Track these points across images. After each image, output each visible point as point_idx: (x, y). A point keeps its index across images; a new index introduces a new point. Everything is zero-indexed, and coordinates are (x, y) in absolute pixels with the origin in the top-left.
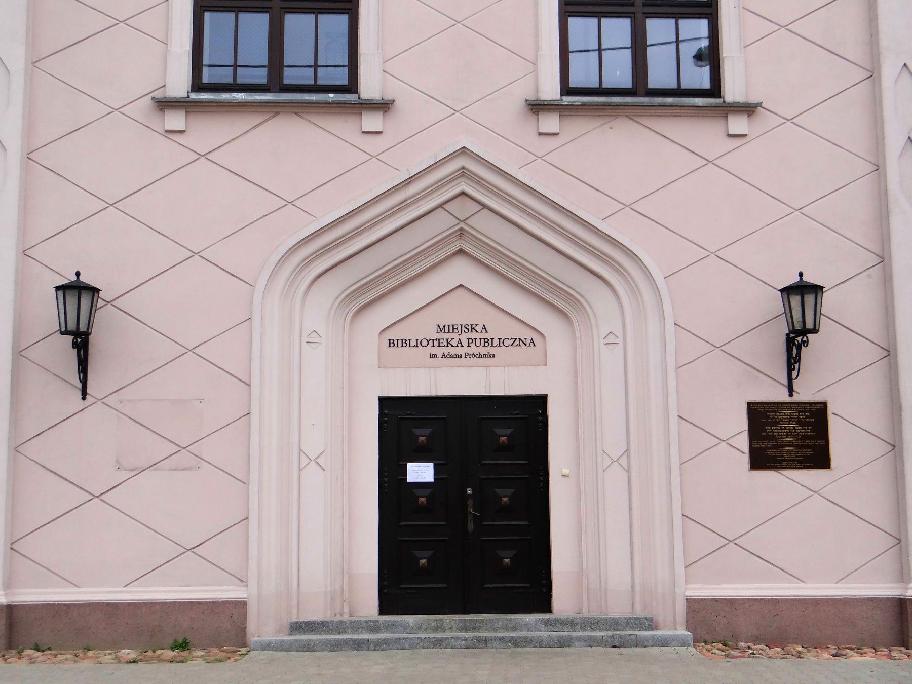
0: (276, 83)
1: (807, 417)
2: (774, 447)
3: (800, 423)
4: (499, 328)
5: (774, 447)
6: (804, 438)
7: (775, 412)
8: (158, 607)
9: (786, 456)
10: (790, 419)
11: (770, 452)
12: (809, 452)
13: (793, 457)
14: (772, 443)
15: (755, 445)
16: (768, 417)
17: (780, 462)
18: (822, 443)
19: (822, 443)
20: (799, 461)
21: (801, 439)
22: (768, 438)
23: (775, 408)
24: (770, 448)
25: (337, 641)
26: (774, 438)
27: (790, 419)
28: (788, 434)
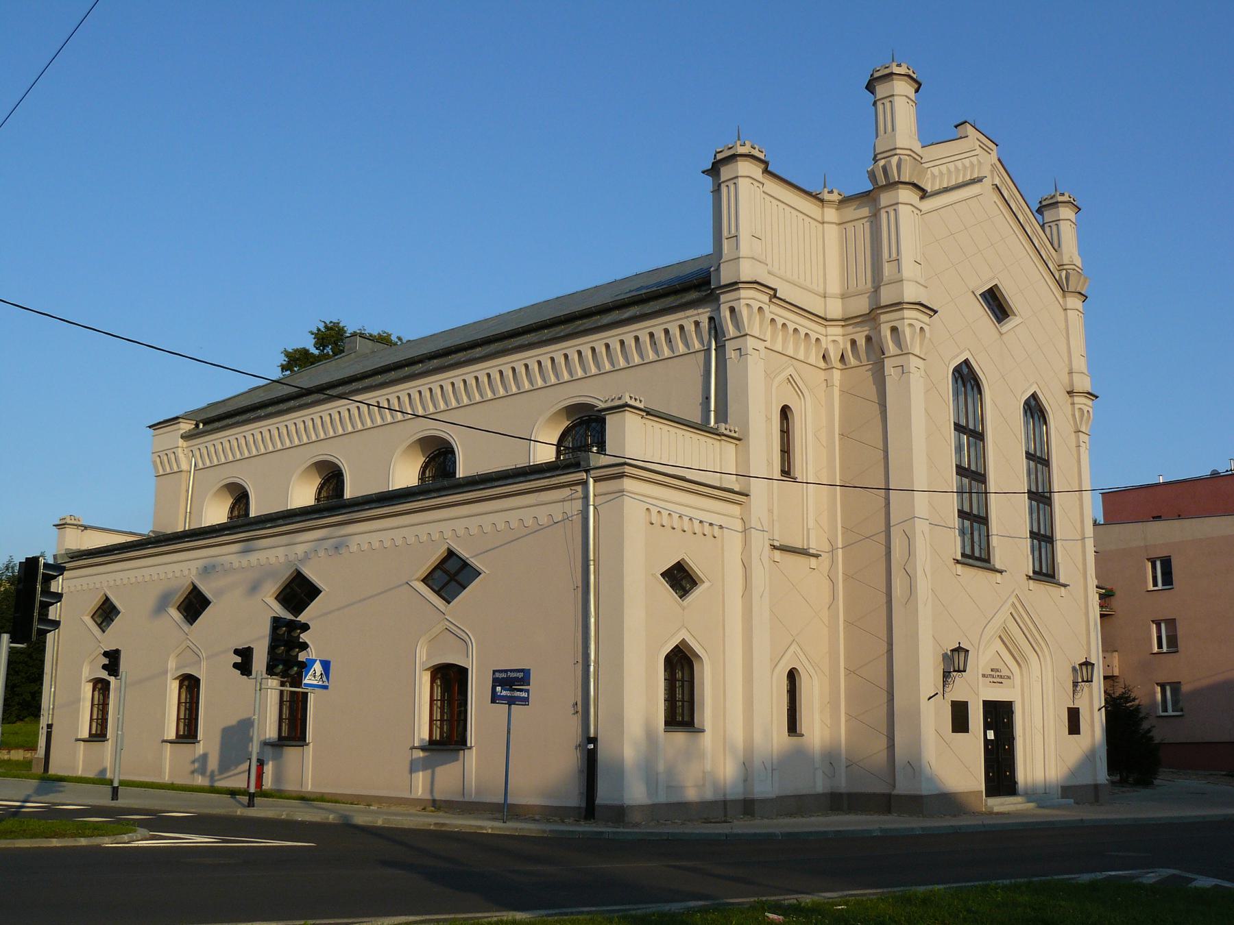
0: (972, 557)
4: (1005, 672)
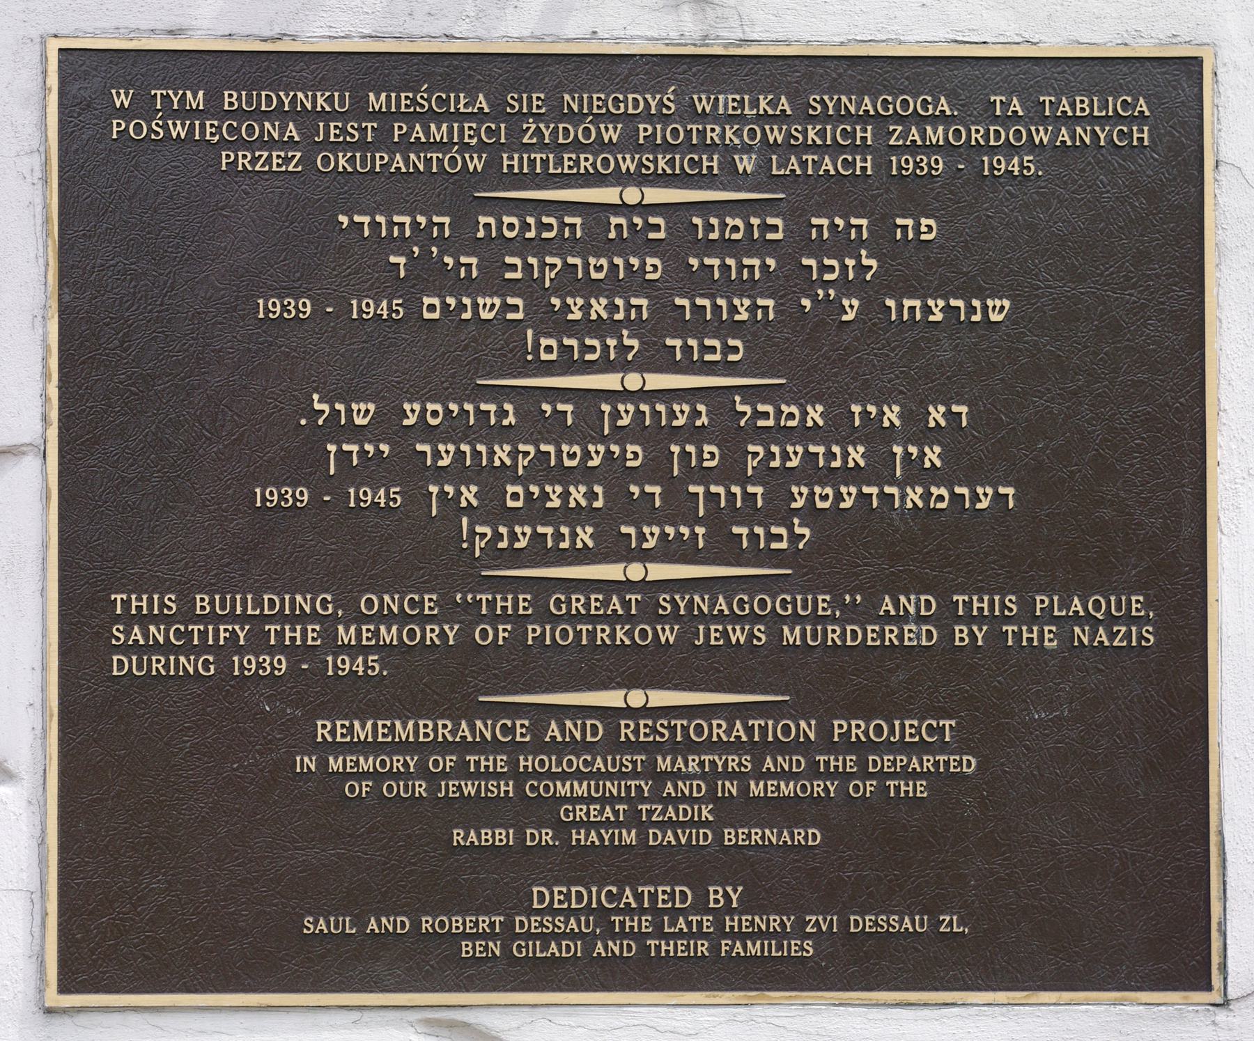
1: (909, 269)
2: (419, 682)
3: (806, 352)
5: (419, 682)
6: (861, 553)
7: (460, 194)
8: (624, 68)
9: (588, 803)
10: (672, 294)
11: (358, 751)
12: (915, 756)
13: (684, 823)
14: (389, 624)
15: (153, 640)
16: (365, 263)
17: (500, 882)
18: (1115, 621)
19: (1115, 621)
20: (765, 880)
21: (808, 568)
22: (356, 555)
23: (453, 139)
24: (355, 698)
25: (539, 187)
26: (426, 554)
27: (672, 294)
28: (618, 501)
